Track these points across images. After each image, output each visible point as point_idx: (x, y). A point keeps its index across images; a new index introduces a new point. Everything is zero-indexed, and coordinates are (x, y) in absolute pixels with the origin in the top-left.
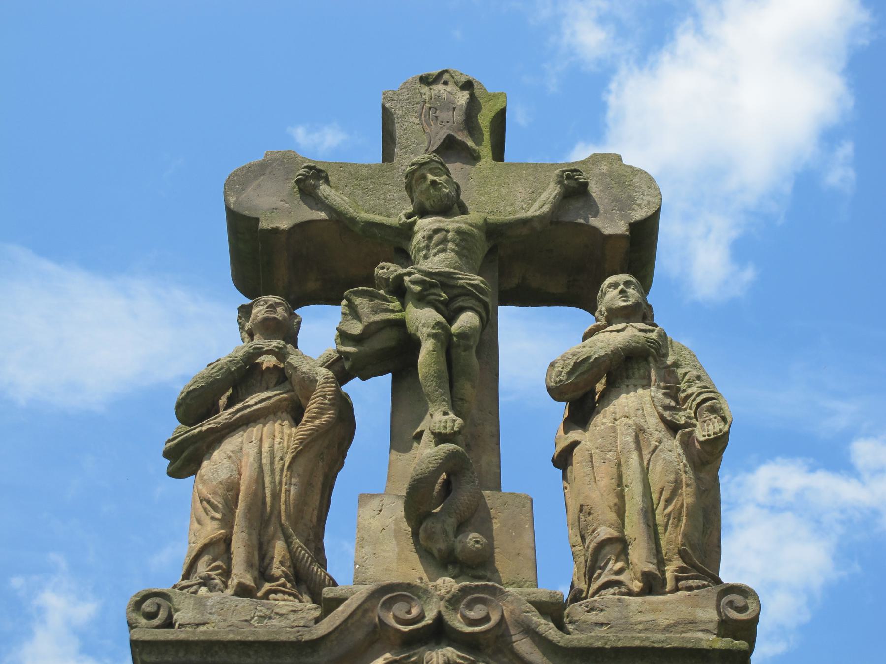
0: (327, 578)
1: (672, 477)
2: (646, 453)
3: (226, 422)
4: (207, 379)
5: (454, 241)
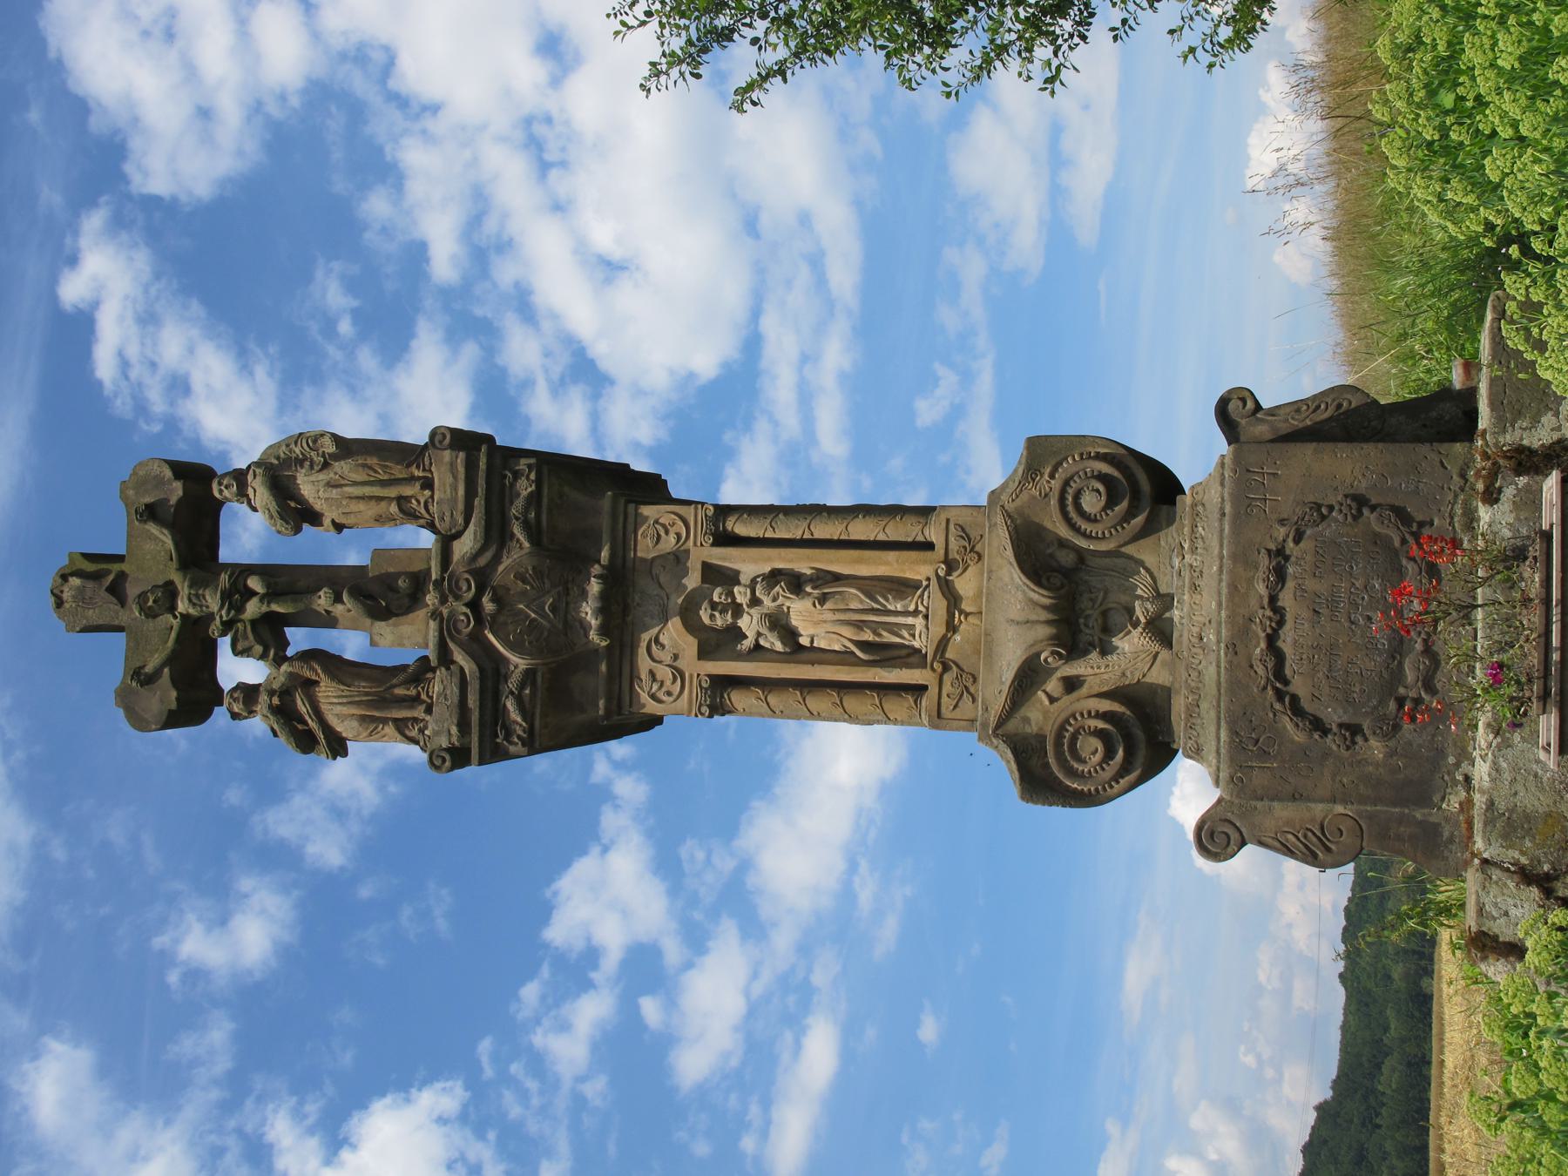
1: (360, 469)
2: (343, 482)
5: (197, 590)
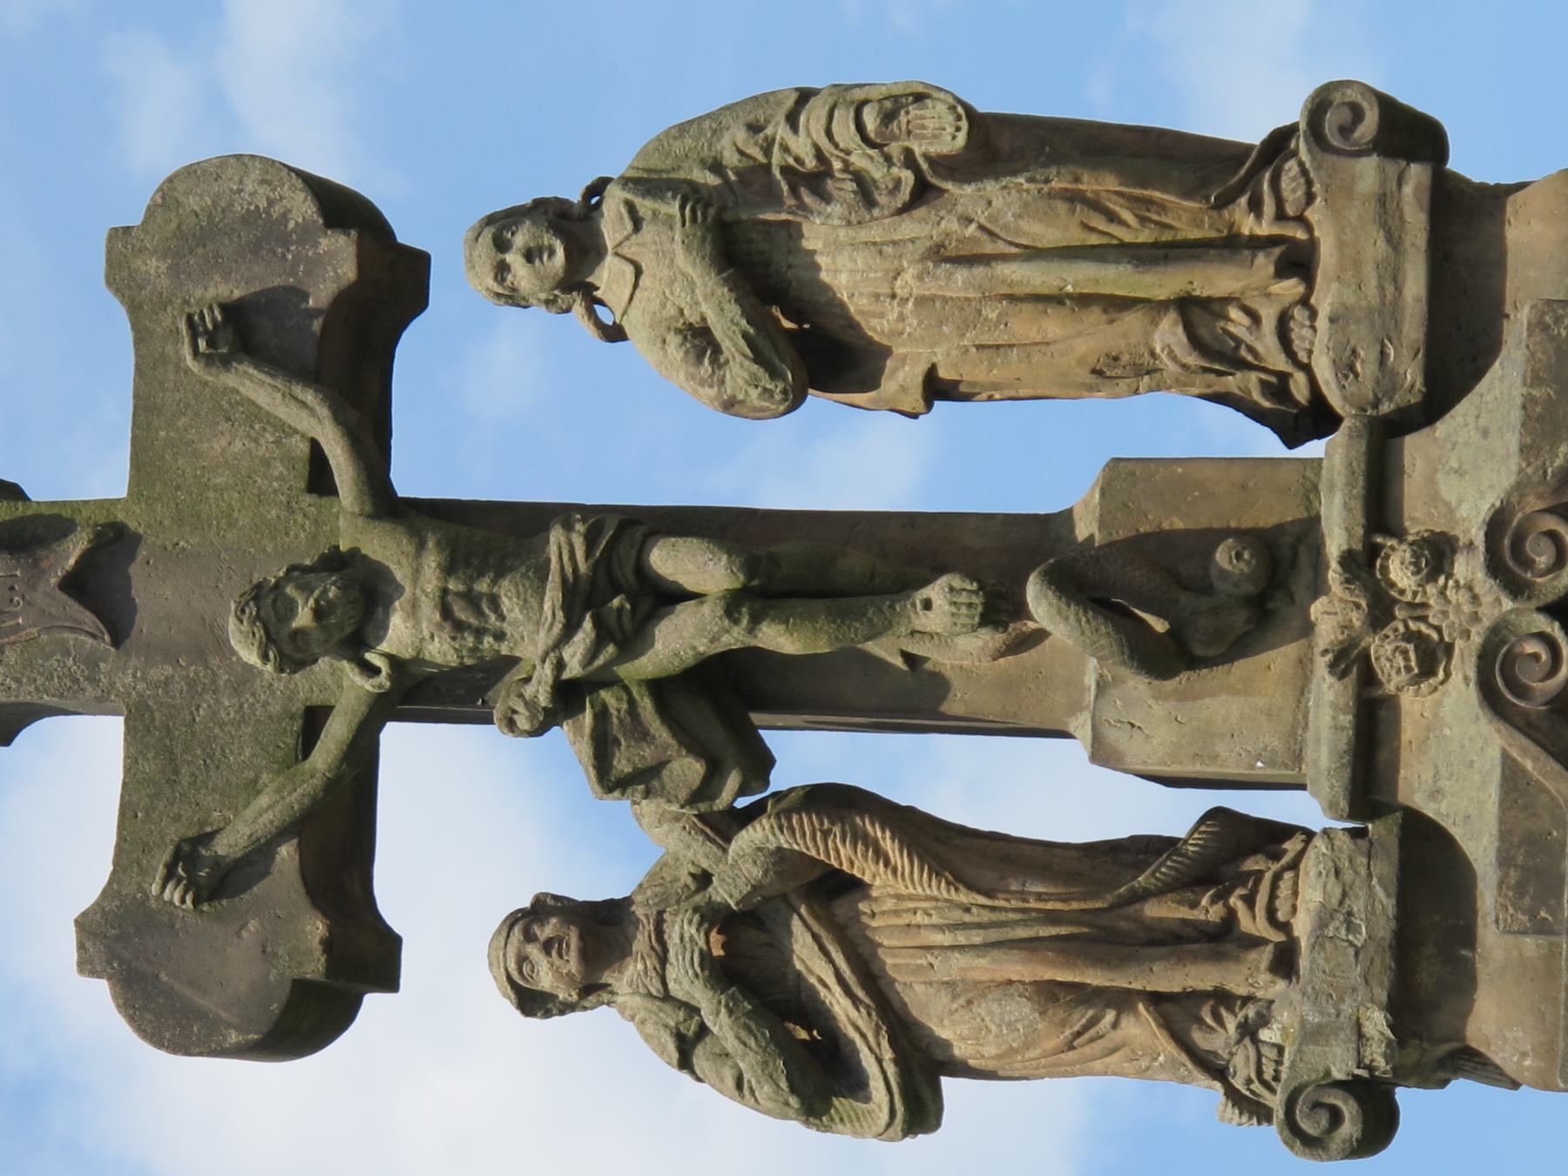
0: (1203, 828)
1: (1061, 207)
2: (988, 247)
3: (877, 1015)
4: (769, 1054)
5: (471, 580)
